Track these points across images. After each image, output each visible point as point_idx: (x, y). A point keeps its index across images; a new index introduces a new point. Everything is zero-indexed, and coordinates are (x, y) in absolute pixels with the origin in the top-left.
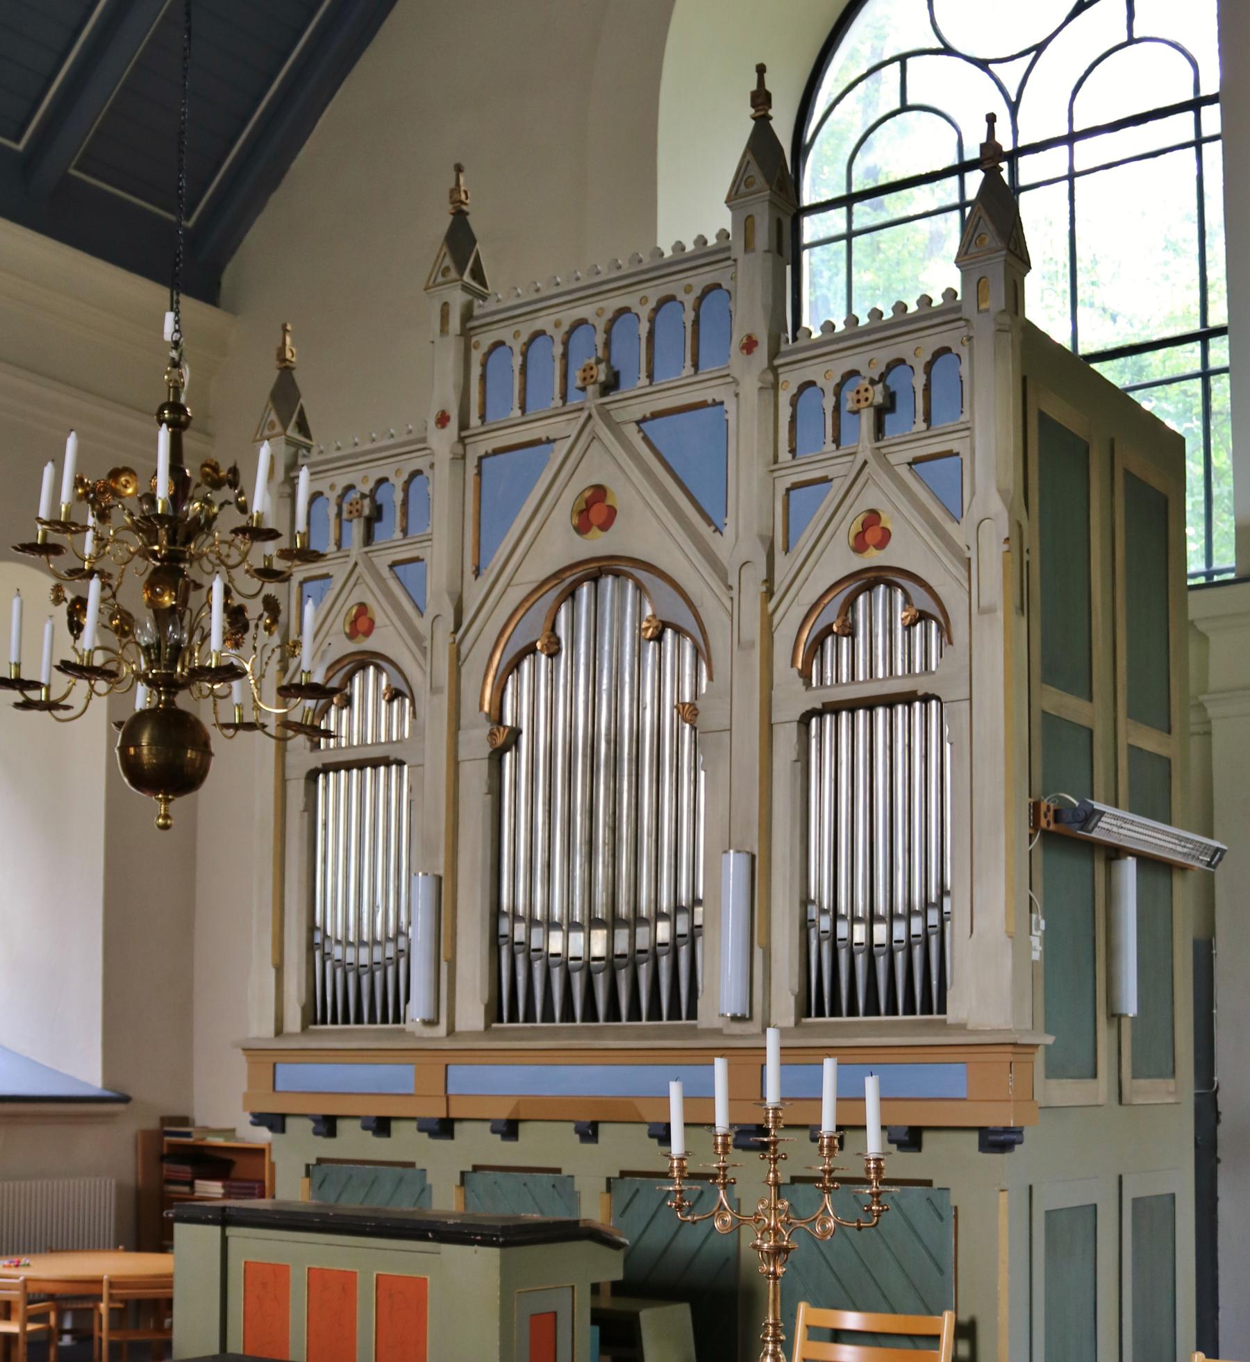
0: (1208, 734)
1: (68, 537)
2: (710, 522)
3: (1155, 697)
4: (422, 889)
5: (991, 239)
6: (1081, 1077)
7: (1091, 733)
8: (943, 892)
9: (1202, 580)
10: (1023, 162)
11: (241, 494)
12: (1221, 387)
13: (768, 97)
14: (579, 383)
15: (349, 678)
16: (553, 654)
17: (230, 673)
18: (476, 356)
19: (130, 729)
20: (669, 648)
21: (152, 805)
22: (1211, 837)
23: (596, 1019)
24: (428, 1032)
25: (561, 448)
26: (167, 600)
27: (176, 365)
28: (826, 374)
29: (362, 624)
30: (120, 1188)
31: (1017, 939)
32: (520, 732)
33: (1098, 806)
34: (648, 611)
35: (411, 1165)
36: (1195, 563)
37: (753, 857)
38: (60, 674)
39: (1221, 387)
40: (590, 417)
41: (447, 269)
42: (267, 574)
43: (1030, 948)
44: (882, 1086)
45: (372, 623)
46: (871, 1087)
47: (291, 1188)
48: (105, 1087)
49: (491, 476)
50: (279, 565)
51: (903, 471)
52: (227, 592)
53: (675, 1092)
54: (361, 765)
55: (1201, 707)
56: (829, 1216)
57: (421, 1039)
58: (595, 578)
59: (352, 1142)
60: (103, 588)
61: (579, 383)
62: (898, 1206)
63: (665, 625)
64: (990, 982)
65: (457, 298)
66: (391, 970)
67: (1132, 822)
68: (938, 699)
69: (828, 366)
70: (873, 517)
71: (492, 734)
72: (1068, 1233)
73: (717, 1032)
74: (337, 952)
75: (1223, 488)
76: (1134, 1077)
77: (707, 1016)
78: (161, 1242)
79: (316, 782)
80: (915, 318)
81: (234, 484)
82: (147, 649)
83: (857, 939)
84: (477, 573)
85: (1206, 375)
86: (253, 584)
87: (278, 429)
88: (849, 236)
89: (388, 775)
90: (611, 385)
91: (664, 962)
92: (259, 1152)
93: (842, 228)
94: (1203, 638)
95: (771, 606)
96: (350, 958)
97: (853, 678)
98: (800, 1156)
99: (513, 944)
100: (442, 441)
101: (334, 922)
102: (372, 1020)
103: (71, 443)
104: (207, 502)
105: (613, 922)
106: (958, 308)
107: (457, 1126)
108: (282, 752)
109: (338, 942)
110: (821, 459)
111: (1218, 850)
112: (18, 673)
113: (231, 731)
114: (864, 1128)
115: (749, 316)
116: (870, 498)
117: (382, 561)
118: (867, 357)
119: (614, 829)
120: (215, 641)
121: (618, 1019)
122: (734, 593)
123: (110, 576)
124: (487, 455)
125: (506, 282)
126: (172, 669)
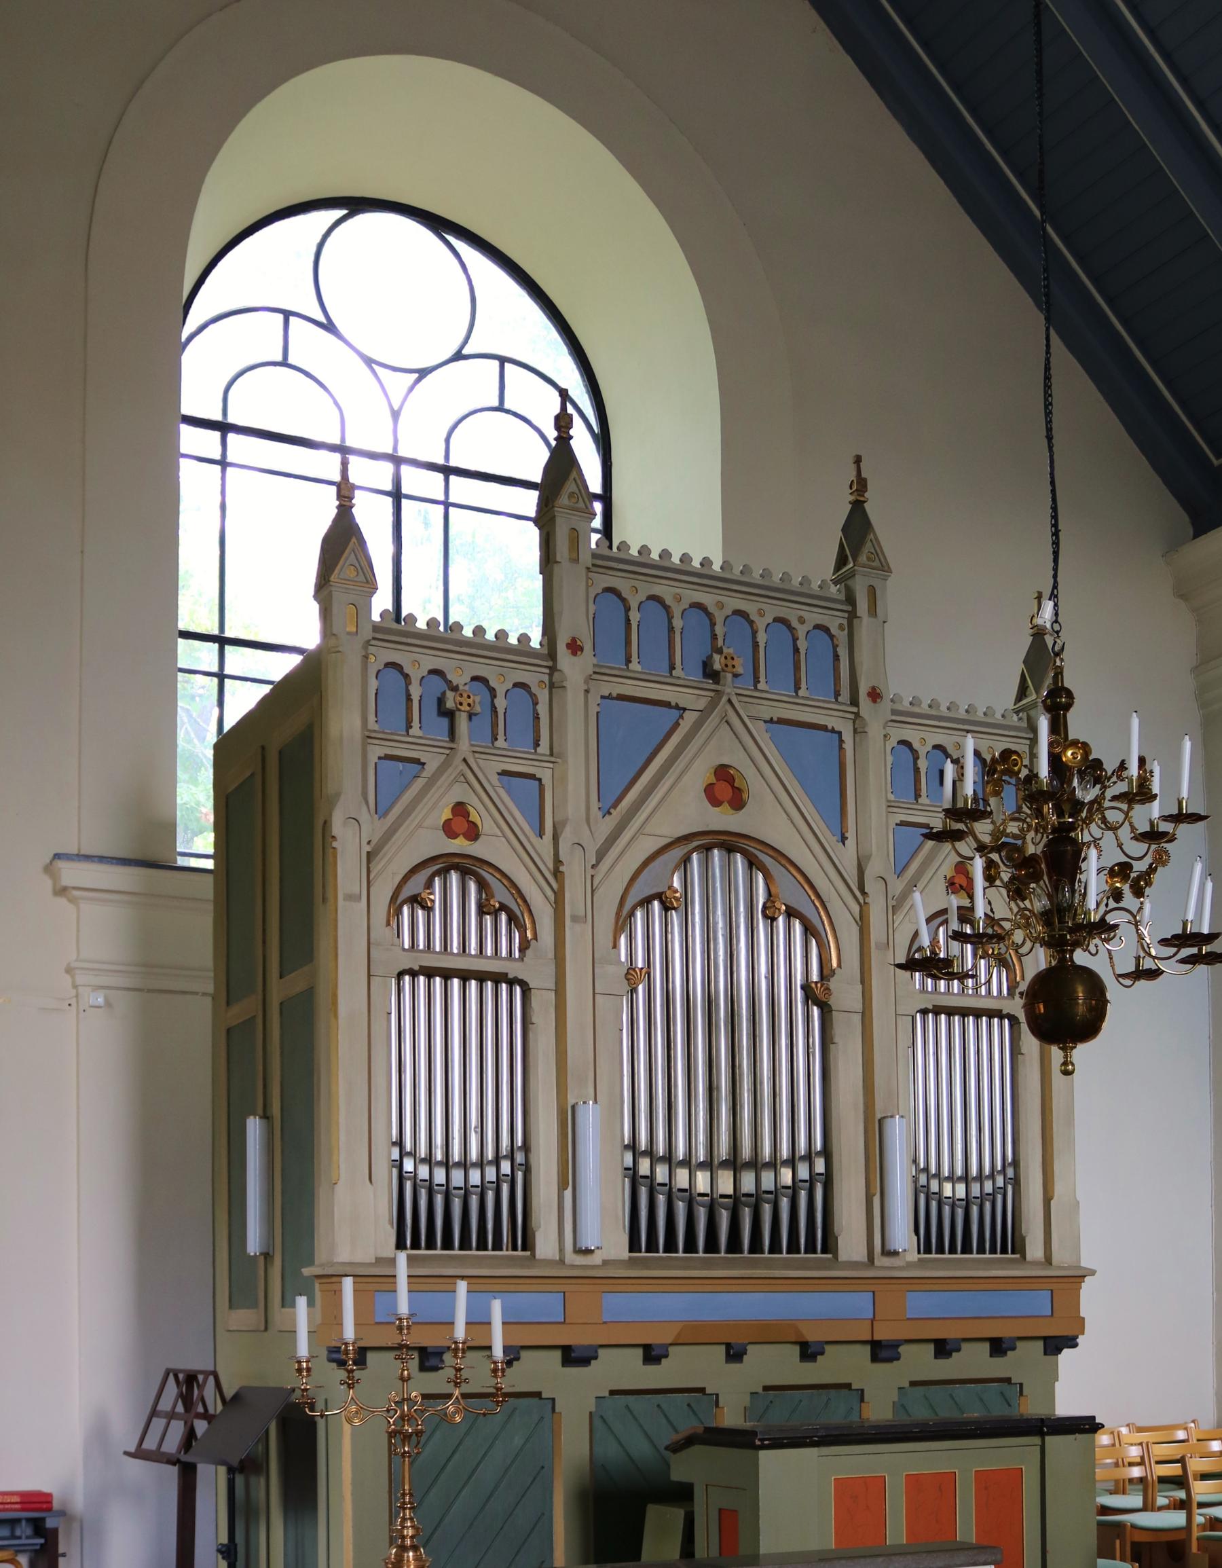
41: (571, 495)
46: (497, 1307)
57: (573, 1266)
66: (988, 1206)
89: (990, 1027)
91: (785, 1203)
97: (464, 951)
105: (734, 1164)
113: (1128, 982)
118: (923, 735)
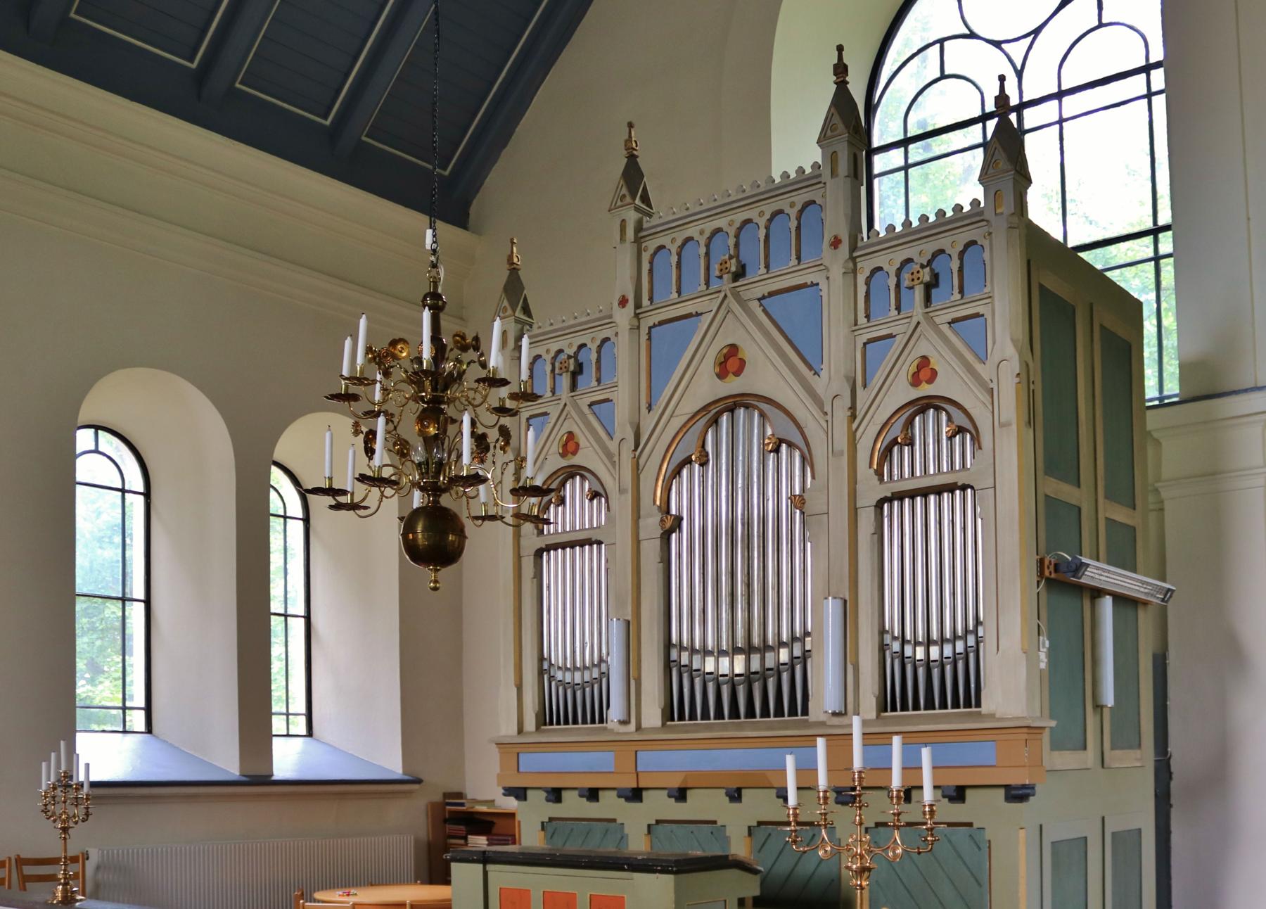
0: (1162, 510)
1: (362, 388)
2: (810, 368)
3: (1124, 486)
4: (616, 628)
5: (1003, 163)
6: (1075, 749)
7: (1080, 509)
8: (978, 622)
9: (1157, 403)
10: (1027, 113)
11: (482, 355)
12: (1168, 267)
13: (846, 67)
14: (717, 273)
15: (563, 484)
16: (703, 464)
17: (476, 480)
18: (646, 257)
19: (409, 523)
20: (784, 457)
21: (426, 573)
22: (1164, 581)
23: (738, 717)
24: (623, 729)
25: (707, 319)
26: (432, 430)
27: (434, 266)
28: (890, 261)
29: (571, 446)
30: (417, 841)
31: (1029, 654)
32: (682, 519)
33: (1084, 560)
34: (769, 432)
35: (614, 820)
36: (1151, 391)
37: (845, 601)
38: (359, 484)
39: (1168, 267)
40: (726, 296)
41: (624, 196)
42: (501, 410)
43: (1039, 660)
44: (934, 757)
45: (577, 445)
46: (926, 753)
47: (531, 838)
48: (404, 773)
49: (658, 337)
50: (509, 404)
51: (945, 328)
52: (473, 424)
53: (790, 761)
54: (572, 545)
55: (1156, 491)
56: (898, 845)
57: (618, 733)
58: (731, 410)
59: (573, 805)
60: (387, 423)
61: (717, 273)
62: (950, 841)
63: (781, 441)
64: (1012, 683)
65: (632, 216)
66: (596, 687)
67: (1109, 571)
68: (972, 488)
69: (891, 256)
70: (924, 361)
71: (662, 520)
72: (1067, 857)
73: (823, 724)
74: (559, 675)
75: (1171, 342)
76: (1112, 749)
77: (815, 713)
78: (444, 878)
79: (541, 557)
80: (951, 221)
81: (476, 348)
82: (419, 465)
83: (918, 657)
84: (650, 408)
85: (1157, 259)
86: (491, 419)
87: (510, 312)
88: (906, 168)
90: (740, 274)
91: (785, 676)
92: (512, 815)
93: (901, 162)
94: (1158, 443)
95: (855, 426)
96: (568, 679)
98: (879, 807)
99: (680, 666)
100: (623, 317)
101: (557, 653)
102: (585, 722)
103: (363, 322)
104: (458, 361)
105: (749, 650)
106: (981, 213)
107: (645, 794)
108: (517, 536)
109: (559, 668)
110: (888, 322)
111: (1169, 590)
112: (331, 484)
114: (921, 788)
115: (835, 224)
116: (923, 348)
117: (584, 402)
119: (749, 585)
120: (466, 459)
121: (754, 716)
122: (829, 418)
123: (392, 415)
124: (655, 326)
125: (665, 206)
126: (437, 478)
